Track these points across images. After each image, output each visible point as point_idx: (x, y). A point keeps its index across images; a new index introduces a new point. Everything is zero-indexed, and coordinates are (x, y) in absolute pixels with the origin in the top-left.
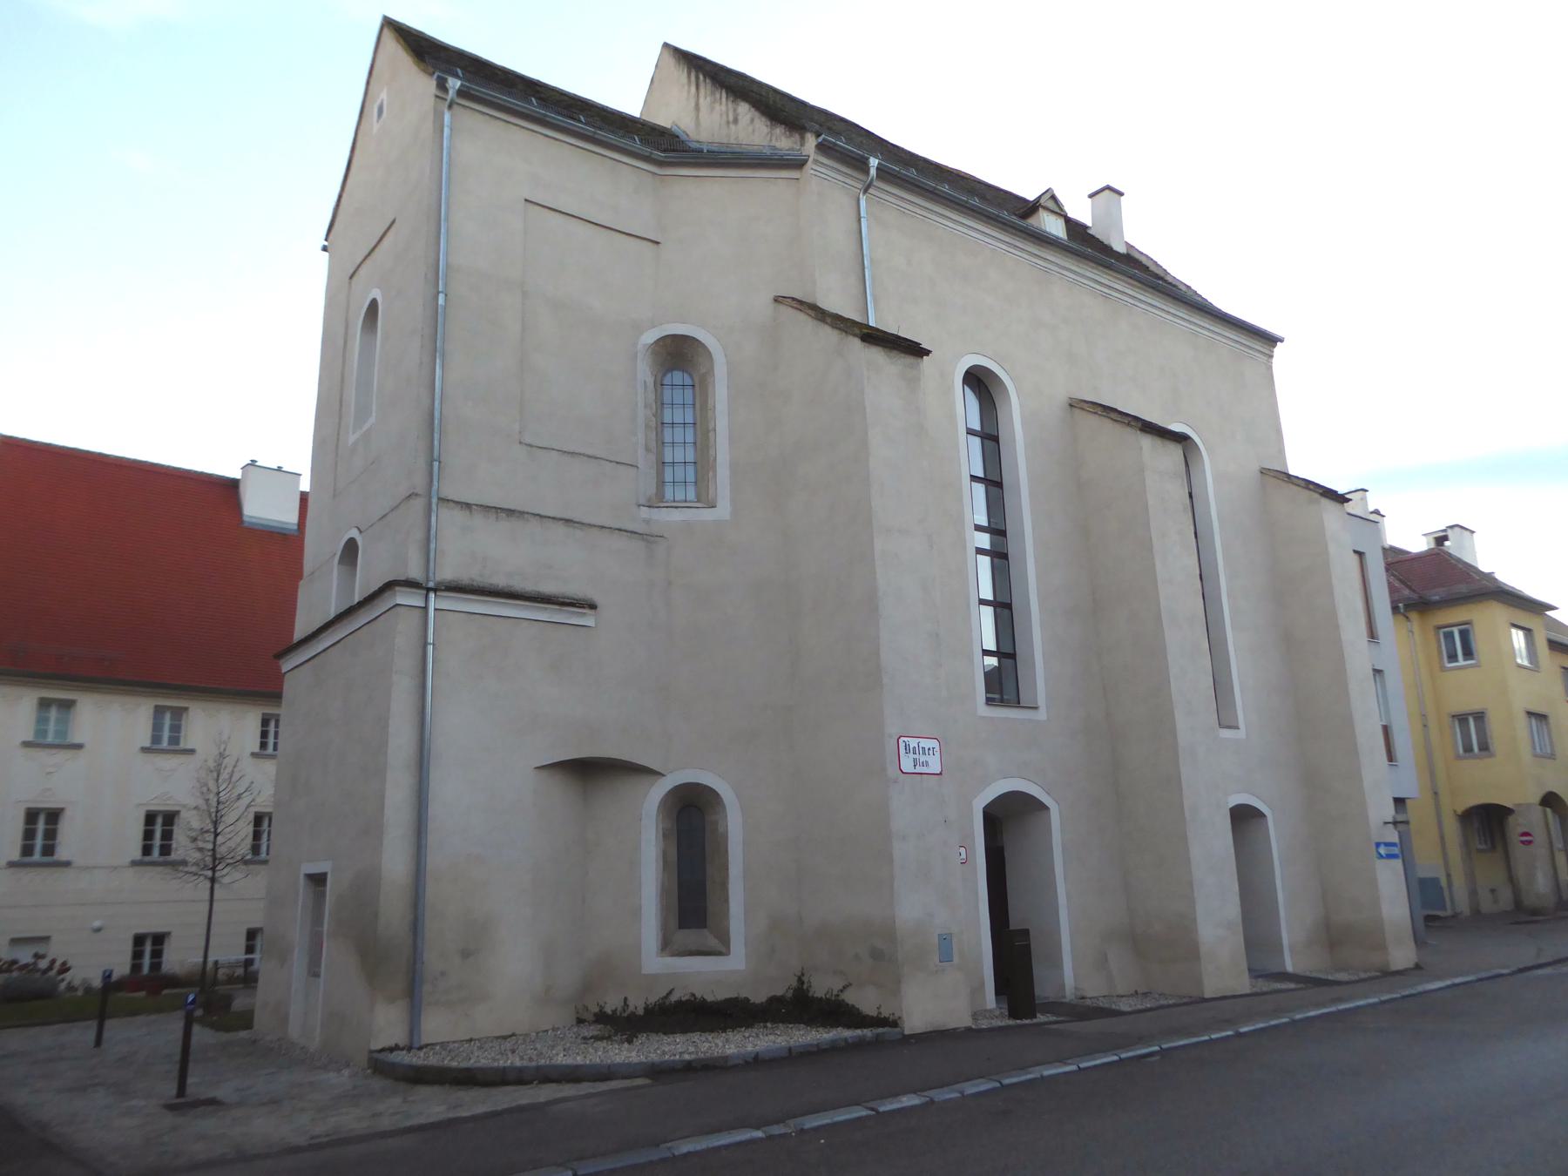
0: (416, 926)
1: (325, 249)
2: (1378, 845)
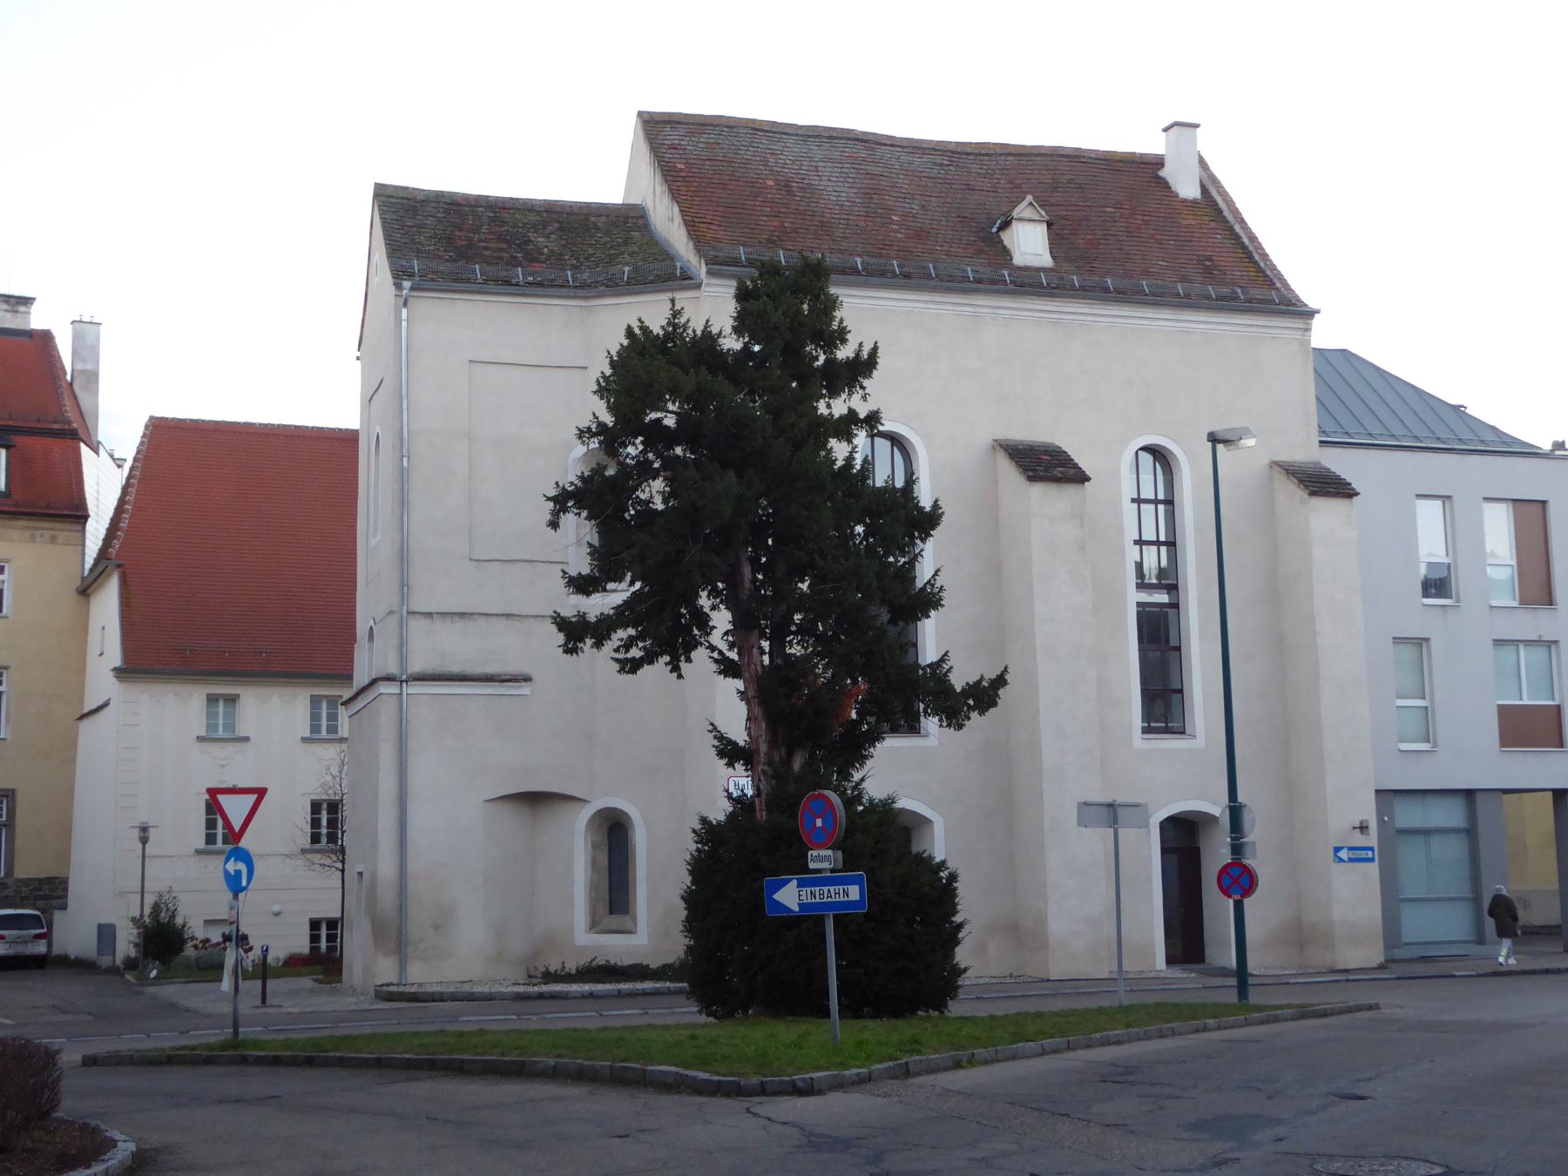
0: (402, 908)
2: (1337, 849)
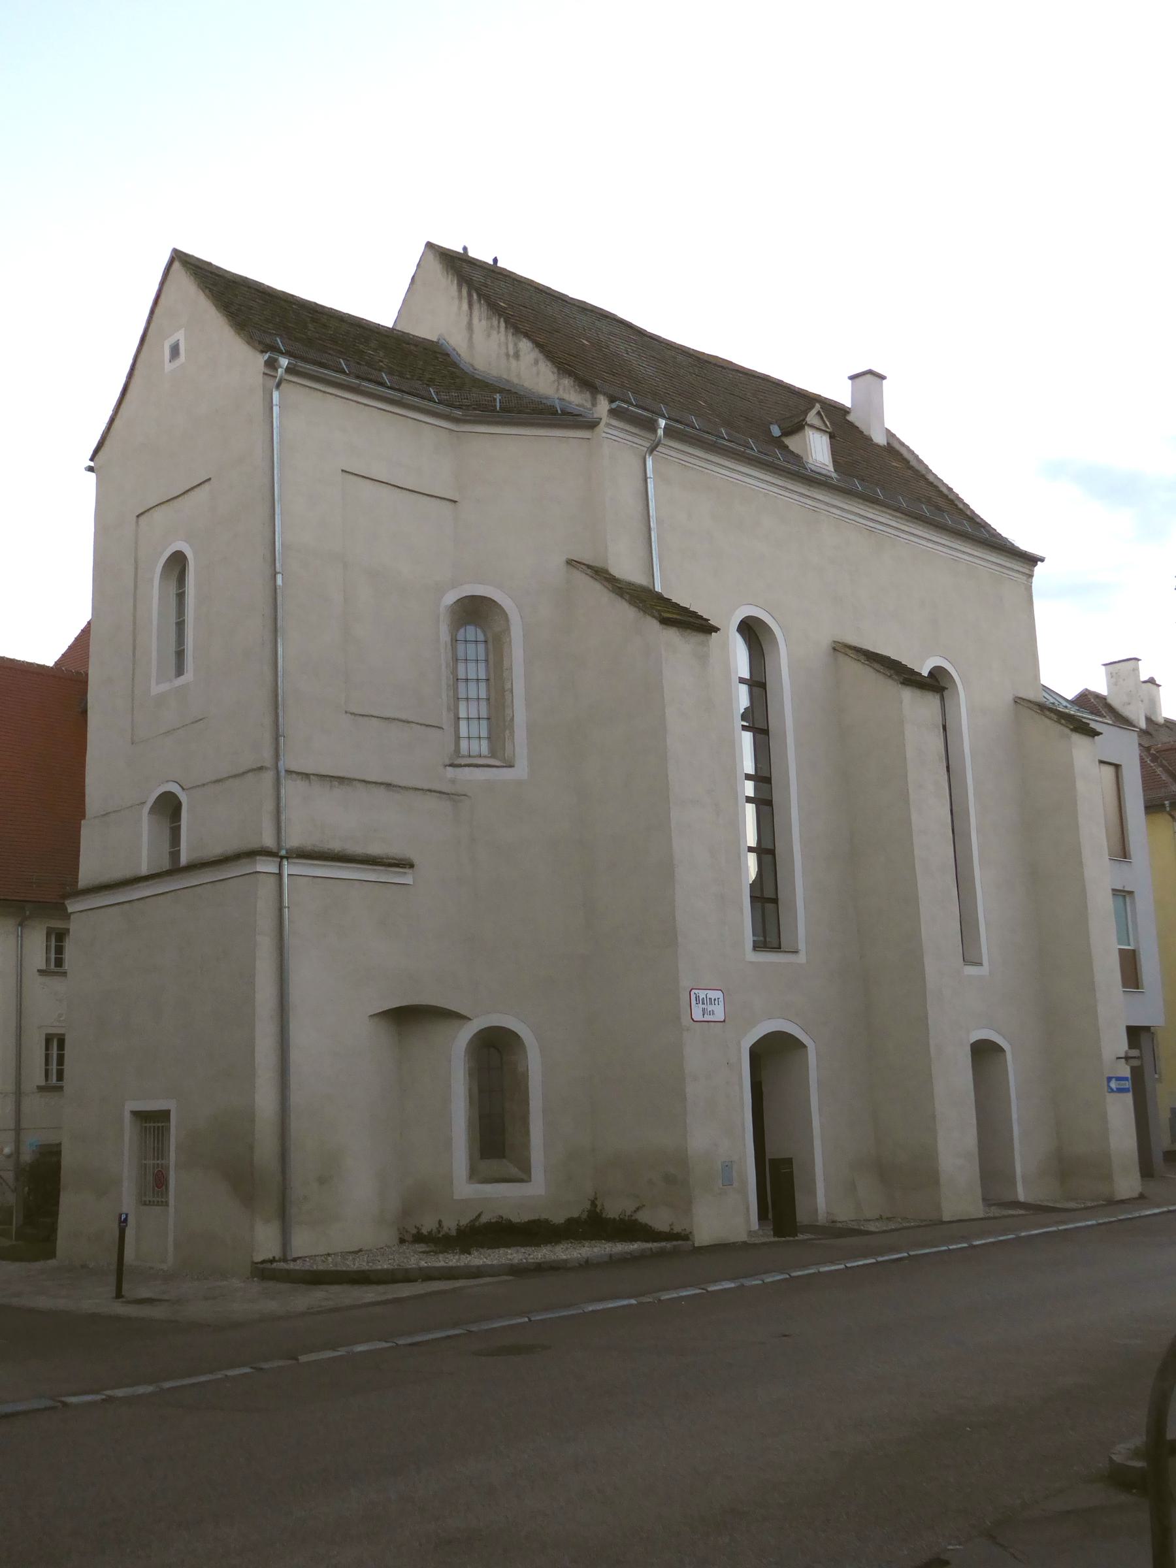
0: (284, 1155)
1: (90, 469)
2: (1109, 1079)
